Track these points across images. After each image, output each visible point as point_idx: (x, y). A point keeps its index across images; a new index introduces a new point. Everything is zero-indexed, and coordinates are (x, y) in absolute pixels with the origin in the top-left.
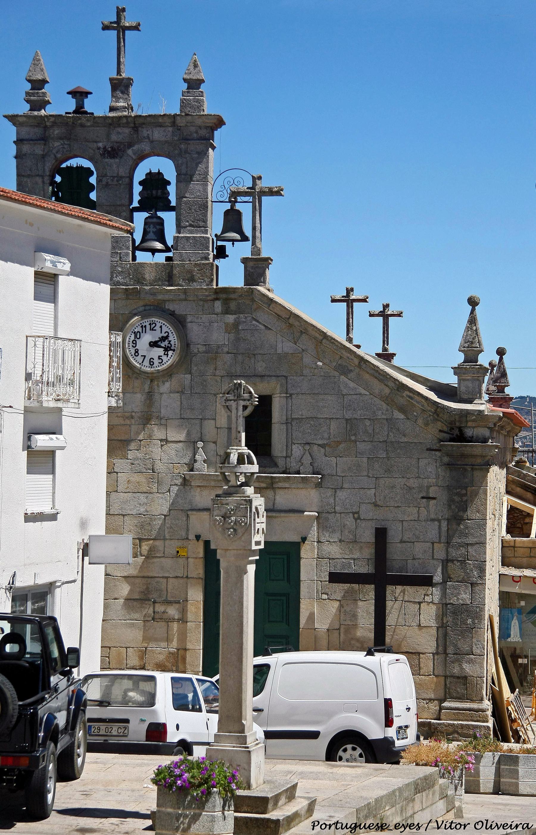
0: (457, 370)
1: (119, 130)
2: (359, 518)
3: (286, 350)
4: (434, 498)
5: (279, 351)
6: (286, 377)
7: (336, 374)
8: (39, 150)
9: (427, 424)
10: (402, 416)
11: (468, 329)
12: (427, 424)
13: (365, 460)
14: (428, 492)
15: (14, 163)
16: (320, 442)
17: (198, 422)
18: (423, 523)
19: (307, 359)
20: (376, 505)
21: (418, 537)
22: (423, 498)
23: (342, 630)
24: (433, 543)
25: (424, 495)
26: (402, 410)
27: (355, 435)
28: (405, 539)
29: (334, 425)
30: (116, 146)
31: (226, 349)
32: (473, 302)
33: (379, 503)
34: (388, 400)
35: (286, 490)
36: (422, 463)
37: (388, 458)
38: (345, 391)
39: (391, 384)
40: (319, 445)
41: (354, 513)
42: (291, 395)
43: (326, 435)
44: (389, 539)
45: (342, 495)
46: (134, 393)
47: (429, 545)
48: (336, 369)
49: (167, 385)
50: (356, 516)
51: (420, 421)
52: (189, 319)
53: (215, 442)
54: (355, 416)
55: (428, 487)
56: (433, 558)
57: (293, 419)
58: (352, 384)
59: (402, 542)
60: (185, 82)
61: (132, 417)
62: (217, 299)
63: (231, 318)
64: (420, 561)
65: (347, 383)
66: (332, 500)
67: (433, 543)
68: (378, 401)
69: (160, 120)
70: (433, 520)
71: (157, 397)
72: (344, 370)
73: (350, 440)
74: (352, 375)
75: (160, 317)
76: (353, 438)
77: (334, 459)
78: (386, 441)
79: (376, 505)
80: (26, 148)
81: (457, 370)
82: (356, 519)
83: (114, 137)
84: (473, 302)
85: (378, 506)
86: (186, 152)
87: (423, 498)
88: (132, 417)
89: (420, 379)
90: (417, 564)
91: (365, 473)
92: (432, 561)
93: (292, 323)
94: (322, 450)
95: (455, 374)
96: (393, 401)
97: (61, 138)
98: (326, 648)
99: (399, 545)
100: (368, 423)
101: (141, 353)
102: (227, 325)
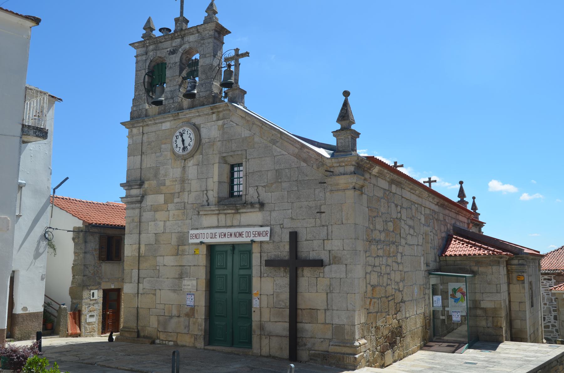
0: (335, 133)
1: (176, 40)
2: (283, 227)
3: (246, 135)
4: (324, 212)
5: (243, 136)
6: (246, 150)
7: (271, 145)
8: (144, 58)
9: (318, 168)
10: (305, 165)
11: (342, 109)
12: (318, 168)
13: (286, 193)
14: (320, 209)
15: (134, 65)
16: (263, 185)
17: (205, 180)
18: (318, 228)
19: (257, 139)
20: (292, 219)
21: (315, 237)
22: (318, 213)
23: (275, 295)
24: (324, 240)
25: (318, 211)
26: (305, 161)
27: (281, 178)
28: (308, 238)
29: (270, 174)
30: (175, 48)
31: (218, 139)
32: (461, 183)
33: (294, 217)
34: (298, 156)
35: (246, 214)
36: (317, 191)
37: (298, 191)
38: (275, 154)
39: (297, 146)
40: (262, 186)
41: (280, 225)
42: (248, 159)
43: (266, 180)
44: (299, 239)
45: (274, 214)
46: (177, 168)
47: (322, 241)
48: (270, 142)
49: (192, 162)
50: (282, 226)
51: (315, 166)
52: (202, 126)
53: (213, 190)
54: (281, 168)
55: (321, 206)
56: (324, 250)
57: (249, 173)
58: (279, 150)
59: (306, 240)
60: (339, 120)
61: (176, 181)
62: (213, 113)
63: (220, 123)
64: (317, 252)
65: (277, 150)
66: (269, 218)
67: (324, 240)
68: (293, 158)
69: (191, 31)
70: (323, 226)
71: (187, 169)
72: (274, 142)
73: (278, 182)
74: (278, 144)
75: (187, 127)
76: (280, 180)
77: (270, 194)
78: (297, 180)
79: (292, 219)
80: (139, 58)
81: (335, 133)
82: (281, 228)
83: (174, 44)
84: (461, 183)
85: (293, 219)
86: (203, 44)
87: (318, 213)
88: (176, 181)
89: (316, 144)
90: (315, 254)
91: (286, 201)
92: (323, 252)
93: (160, 37)
94: (264, 189)
95: (334, 136)
96: (300, 156)
97: (153, 50)
98: (218, 249)
99: (305, 242)
100: (287, 171)
101: (178, 146)
102: (219, 126)
